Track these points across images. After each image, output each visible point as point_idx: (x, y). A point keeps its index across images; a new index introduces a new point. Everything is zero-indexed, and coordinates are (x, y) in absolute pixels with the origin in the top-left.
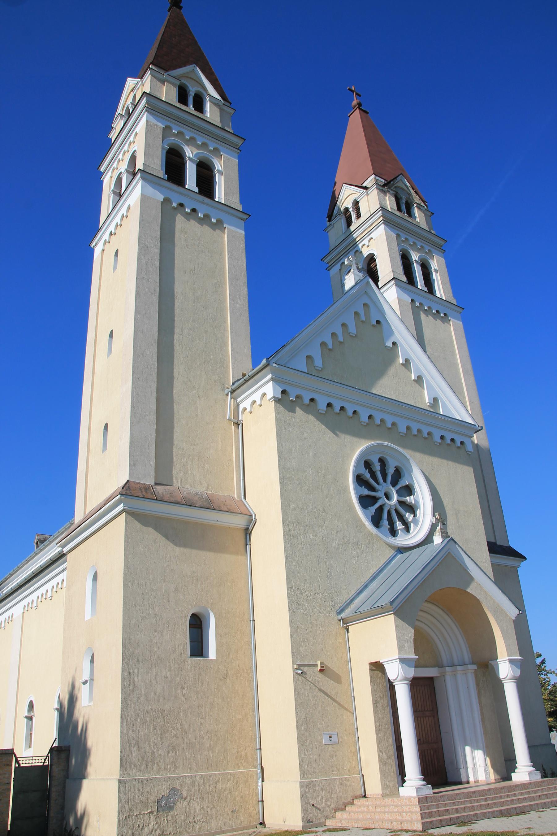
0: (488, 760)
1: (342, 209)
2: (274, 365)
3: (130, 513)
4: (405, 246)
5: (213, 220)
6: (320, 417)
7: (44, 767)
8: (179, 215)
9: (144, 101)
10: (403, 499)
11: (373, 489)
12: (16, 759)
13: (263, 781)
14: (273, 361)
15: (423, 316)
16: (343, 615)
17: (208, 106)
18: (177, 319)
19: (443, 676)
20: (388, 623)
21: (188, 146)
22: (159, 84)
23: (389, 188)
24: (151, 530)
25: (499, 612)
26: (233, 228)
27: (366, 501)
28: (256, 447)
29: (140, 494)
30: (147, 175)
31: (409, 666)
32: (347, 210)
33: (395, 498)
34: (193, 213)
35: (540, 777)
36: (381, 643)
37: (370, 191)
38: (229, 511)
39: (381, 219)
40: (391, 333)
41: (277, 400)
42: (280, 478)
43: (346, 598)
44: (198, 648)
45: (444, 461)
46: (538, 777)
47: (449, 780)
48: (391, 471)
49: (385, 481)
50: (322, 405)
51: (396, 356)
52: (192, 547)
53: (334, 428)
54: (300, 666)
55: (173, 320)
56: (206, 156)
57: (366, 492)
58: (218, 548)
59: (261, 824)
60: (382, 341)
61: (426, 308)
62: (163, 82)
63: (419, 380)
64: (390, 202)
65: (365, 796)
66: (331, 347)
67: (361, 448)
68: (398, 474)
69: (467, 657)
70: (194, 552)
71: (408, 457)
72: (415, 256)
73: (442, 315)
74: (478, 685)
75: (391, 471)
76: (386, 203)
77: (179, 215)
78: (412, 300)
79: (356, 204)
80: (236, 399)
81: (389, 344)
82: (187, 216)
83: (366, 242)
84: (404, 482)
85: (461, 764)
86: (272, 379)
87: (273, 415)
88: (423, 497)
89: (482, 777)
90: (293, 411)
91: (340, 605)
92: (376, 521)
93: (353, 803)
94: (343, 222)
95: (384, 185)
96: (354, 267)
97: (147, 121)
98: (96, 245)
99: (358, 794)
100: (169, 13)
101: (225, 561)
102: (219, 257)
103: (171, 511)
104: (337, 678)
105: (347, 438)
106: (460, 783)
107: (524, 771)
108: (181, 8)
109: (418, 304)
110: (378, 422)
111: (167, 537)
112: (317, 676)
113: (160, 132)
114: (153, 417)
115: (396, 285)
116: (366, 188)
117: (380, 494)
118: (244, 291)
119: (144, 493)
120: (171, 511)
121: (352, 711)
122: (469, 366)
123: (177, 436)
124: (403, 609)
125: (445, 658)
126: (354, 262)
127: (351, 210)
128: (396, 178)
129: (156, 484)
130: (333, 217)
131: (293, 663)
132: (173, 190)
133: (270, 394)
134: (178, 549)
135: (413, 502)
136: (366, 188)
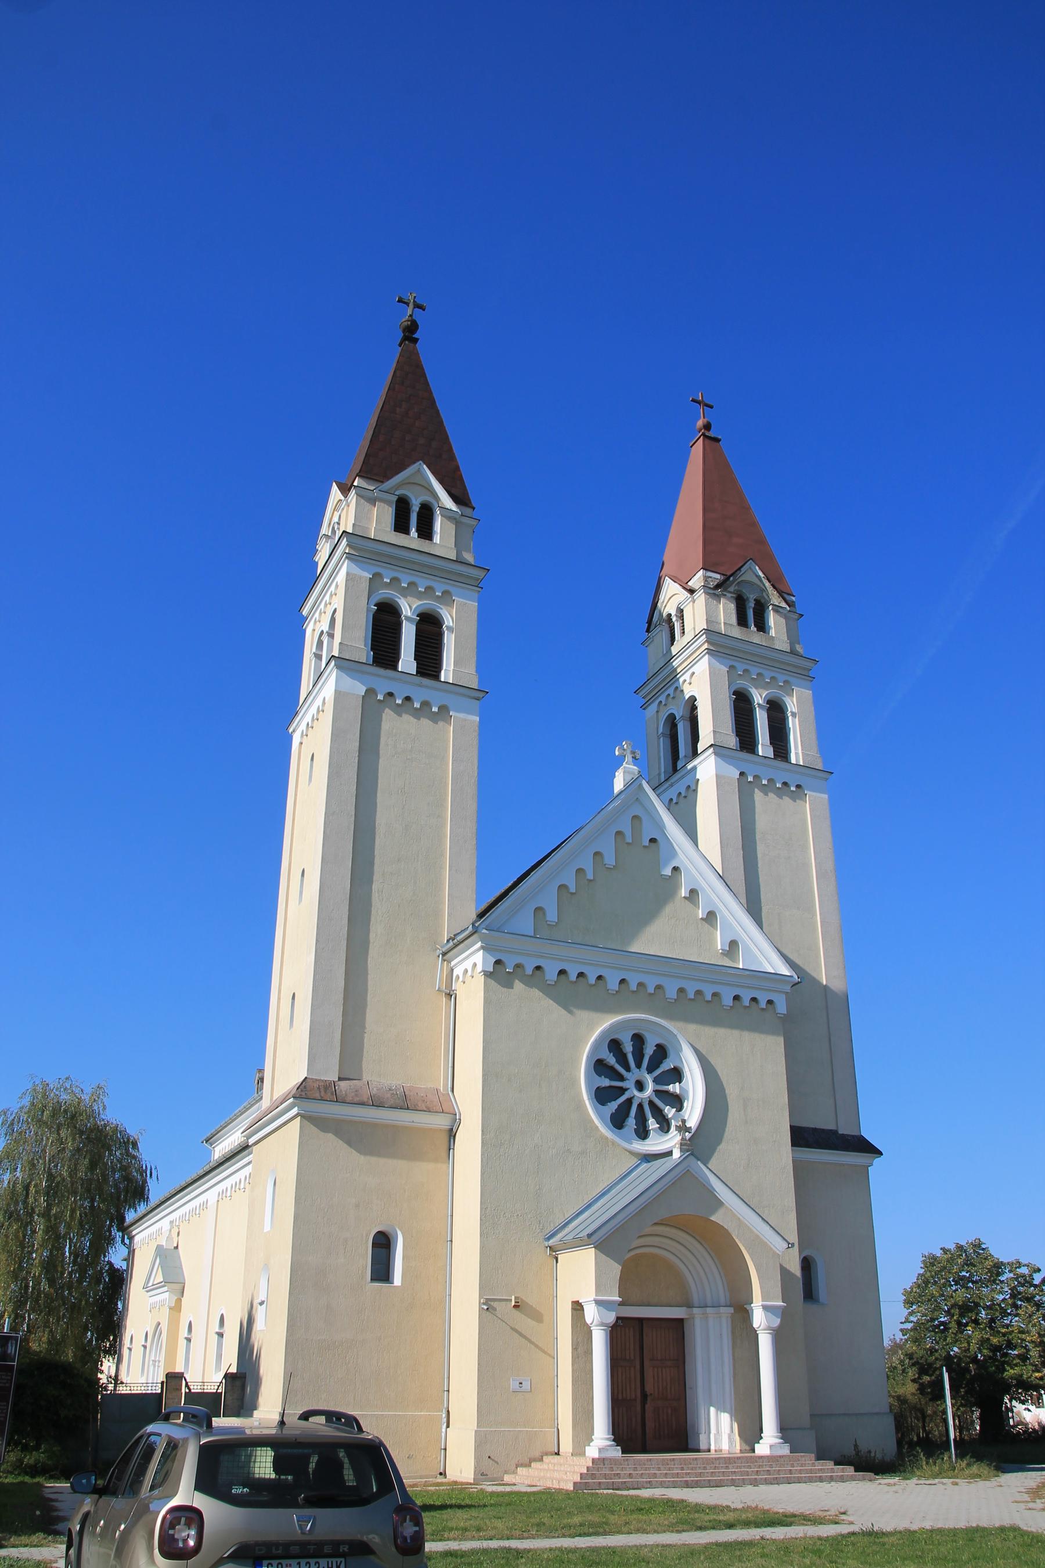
1: (665, 615)
2: (484, 931)
3: (306, 1117)
4: (741, 683)
5: (435, 709)
6: (548, 990)
7: (217, 1395)
8: (387, 710)
9: (344, 542)
10: (664, 1088)
11: (622, 1078)
12: (187, 1383)
13: (448, 1426)
14: (483, 926)
15: (758, 795)
16: (551, 1242)
17: (438, 523)
18: (377, 861)
19: (692, 1317)
20: (588, 1256)
21: (405, 597)
22: (367, 506)
23: (725, 590)
24: (330, 1136)
25: (758, 1245)
26: (461, 715)
27: (602, 1096)
28: (459, 1031)
29: (317, 1095)
30: (342, 662)
32: (670, 615)
33: (650, 1087)
34: (408, 703)
35: (788, 1452)
36: (581, 1280)
37: (696, 595)
38: (429, 1110)
39: (706, 646)
40: (673, 854)
41: (487, 974)
42: (483, 1076)
43: (559, 1220)
44: (382, 1272)
45: (736, 1033)
46: (785, 1450)
47: (690, 1446)
48: (649, 1050)
49: (639, 1066)
50: (551, 974)
51: (676, 887)
52: (379, 1155)
53: (567, 1004)
54: (487, 1302)
55: (372, 864)
56: (428, 606)
57: (606, 1082)
58: (414, 1155)
59: (441, 1474)
61: (765, 782)
62: (372, 501)
63: (711, 917)
64: (725, 611)
65: (558, 1454)
66: (573, 890)
68: (661, 1052)
69: (722, 1296)
70: (382, 1161)
71: (675, 1032)
72: (758, 697)
73: (793, 789)
74: (733, 1333)
75: (649, 1050)
76: (718, 615)
77: (387, 710)
78: (742, 774)
79: (680, 612)
80: (449, 962)
81: (667, 871)
82: (398, 710)
83: (687, 676)
84: (668, 1065)
85: (703, 1427)
86: (482, 948)
87: (481, 994)
88: (694, 1088)
89: (725, 1446)
90: (766, 794)
91: (550, 1229)
92: (618, 1121)
93: (541, 1460)
94: (665, 635)
95: (717, 587)
96: (629, 758)
97: (348, 574)
98: (294, 731)
99: (550, 1450)
100: (400, 349)
101: (421, 1171)
102: (441, 756)
103: (356, 1112)
104: (537, 1316)
105: (583, 1015)
106: (698, 1451)
107: (769, 1442)
108: (416, 340)
109: (750, 779)
110: (633, 987)
111: (349, 1143)
112: (509, 1312)
113: (365, 586)
114: (340, 996)
115: (716, 753)
116: (692, 591)
117: (629, 1084)
118: (471, 806)
119: (323, 1093)
120: (356, 1112)
121: (554, 1357)
122: (830, 865)
124: (605, 1242)
125: (695, 1299)
126: (628, 751)
127: (674, 619)
128: (739, 569)
129: (340, 1079)
130: (652, 627)
131: (480, 1297)
132: (379, 676)
133: (479, 968)
134: (362, 1157)
135: (678, 1091)
136: (692, 591)
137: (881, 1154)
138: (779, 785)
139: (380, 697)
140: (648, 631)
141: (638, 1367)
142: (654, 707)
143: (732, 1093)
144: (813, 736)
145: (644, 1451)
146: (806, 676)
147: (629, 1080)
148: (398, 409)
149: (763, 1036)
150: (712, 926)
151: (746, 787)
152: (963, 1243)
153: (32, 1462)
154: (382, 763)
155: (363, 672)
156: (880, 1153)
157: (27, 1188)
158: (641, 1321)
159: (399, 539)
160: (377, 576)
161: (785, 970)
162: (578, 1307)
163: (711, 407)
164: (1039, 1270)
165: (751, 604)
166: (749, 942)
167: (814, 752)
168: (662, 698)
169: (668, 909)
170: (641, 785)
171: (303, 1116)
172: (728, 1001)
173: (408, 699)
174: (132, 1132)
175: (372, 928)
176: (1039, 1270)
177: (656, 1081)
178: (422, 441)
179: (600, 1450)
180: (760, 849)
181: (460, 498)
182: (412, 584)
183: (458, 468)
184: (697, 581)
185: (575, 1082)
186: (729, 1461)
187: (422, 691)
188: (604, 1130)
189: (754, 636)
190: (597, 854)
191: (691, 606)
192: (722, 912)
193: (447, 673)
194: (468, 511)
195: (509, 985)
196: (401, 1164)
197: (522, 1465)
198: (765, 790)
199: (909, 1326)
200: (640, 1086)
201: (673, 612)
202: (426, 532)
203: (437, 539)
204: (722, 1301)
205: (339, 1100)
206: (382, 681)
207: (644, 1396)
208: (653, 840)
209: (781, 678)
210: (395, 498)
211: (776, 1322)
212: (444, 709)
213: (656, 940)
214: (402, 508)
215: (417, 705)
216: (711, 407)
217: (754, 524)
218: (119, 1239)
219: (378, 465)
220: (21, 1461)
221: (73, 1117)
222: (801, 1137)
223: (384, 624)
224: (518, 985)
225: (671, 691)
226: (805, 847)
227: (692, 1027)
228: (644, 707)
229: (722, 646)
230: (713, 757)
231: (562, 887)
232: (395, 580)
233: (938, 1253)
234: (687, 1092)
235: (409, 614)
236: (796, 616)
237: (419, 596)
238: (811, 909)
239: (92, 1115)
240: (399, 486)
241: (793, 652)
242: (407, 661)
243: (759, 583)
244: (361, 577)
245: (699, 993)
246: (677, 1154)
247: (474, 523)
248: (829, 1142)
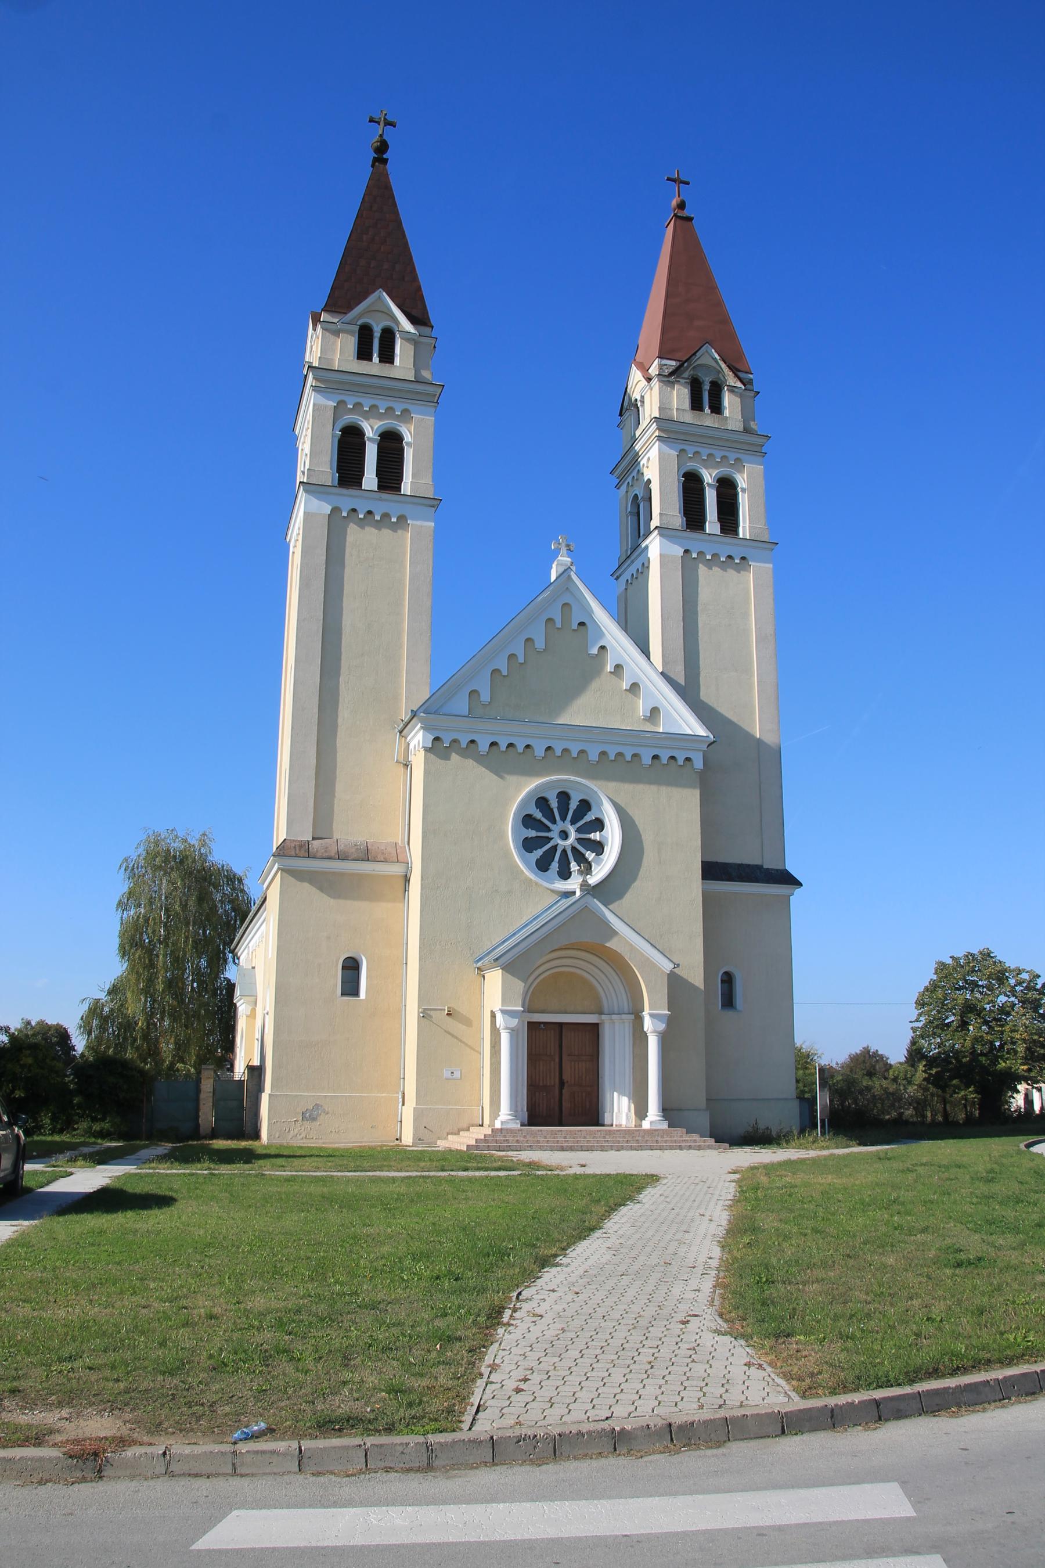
0: (632, 1106)
4: (691, 466)
5: (394, 520)
6: (480, 759)
13: (403, 1104)
15: (702, 569)
16: (479, 964)
18: (343, 657)
20: (495, 978)
21: (367, 419)
22: (332, 337)
24: (306, 885)
25: (648, 964)
26: (418, 523)
27: (528, 845)
29: (293, 853)
31: (513, 1017)
33: (573, 835)
34: (369, 516)
36: (495, 995)
38: (386, 861)
40: (600, 634)
41: (427, 750)
44: (351, 988)
45: (654, 788)
46: (665, 1125)
49: (563, 819)
50: (483, 746)
51: (603, 665)
52: (346, 898)
55: (339, 660)
57: (532, 833)
60: (586, 647)
62: (336, 333)
63: (634, 687)
64: (680, 396)
66: (505, 673)
67: (527, 790)
68: (585, 806)
70: (349, 902)
71: (595, 789)
74: (634, 1035)
76: (671, 402)
77: (351, 525)
78: (686, 551)
79: (642, 397)
81: (595, 651)
82: (362, 524)
84: (590, 817)
86: (422, 728)
88: (613, 835)
89: (624, 1122)
92: (542, 866)
93: (468, 1130)
95: (671, 374)
96: (564, 550)
101: (381, 909)
104: (468, 1022)
105: (512, 779)
106: (603, 1125)
109: (694, 555)
111: (321, 889)
112: (443, 1019)
113: (330, 414)
117: (554, 834)
121: (480, 1053)
122: (770, 629)
123: (339, 787)
128: (695, 354)
129: (314, 839)
131: (419, 1007)
137: (801, 885)
138: (723, 559)
139: (344, 514)
140: (621, 415)
141: (557, 1060)
142: (624, 487)
143: (648, 839)
144: (762, 509)
145: (561, 1124)
146: (758, 452)
147: (554, 832)
148: (365, 237)
149: (680, 790)
150: (635, 695)
151: (689, 563)
152: (975, 952)
153: (98, 1129)
154: (348, 571)
156: (800, 884)
157: (147, 920)
158: (561, 1025)
159: (363, 367)
160: (341, 403)
161: (701, 731)
162: (493, 1015)
163: (688, 183)
164: (1039, 976)
165: (707, 387)
166: (669, 708)
167: (761, 525)
168: (629, 480)
169: (595, 685)
170: (569, 577)
171: (282, 870)
172: (647, 760)
173: (370, 512)
174: (238, 870)
175: (340, 714)
176: (1039, 976)
177: (578, 831)
178: (386, 266)
179: (502, 1123)
180: (702, 619)
181: (419, 319)
182: (373, 407)
183: (419, 289)
184: (654, 370)
185: (502, 835)
186: (628, 1132)
187: (386, 504)
188: (529, 874)
189: (707, 418)
190: (528, 640)
191: (651, 394)
192: (645, 683)
193: (407, 486)
194: (426, 330)
195: (447, 758)
196: (364, 905)
197: (452, 1134)
198: (709, 564)
199: (920, 1024)
200: (564, 835)
201: (639, 399)
202: (387, 357)
203: (397, 361)
204: (626, 1010)
205: (309, 855)
206: (347, 499)
207: (562, 1084)
208: (582, 624)
209: (732, 456)
210: (357, 328)
211: (662, 1027)
212: (402, 519)
213: (583, 712)
214: (365, 334)
215: (377, 518)
216: (688, 183)
217: (719, 304)
218: (230, 959)
219: (342, 298)
220: (91, 1128)
221: (182, 862)
222: (712, 871)
223: (349, 446)
224: (454, 757)
225: (635, 473)
226: (746, 615)
227: (612, 785)
228: (618, 487)
229: (672, 432)
230: (658, 537)
231: (496, 671)
232: (358, 405)
233: (950, 961)
234: (607, 839)
235: (371, 435)
236: (752, 394)
237: (381, 416)
238: (748, 671)
239: (203, 858)
241: (747, 430)
242: (370, 479)
243: (714, 365)
244: (326, 406)
246: (578, 893)
247: (433, 341)
248: (744, 875)
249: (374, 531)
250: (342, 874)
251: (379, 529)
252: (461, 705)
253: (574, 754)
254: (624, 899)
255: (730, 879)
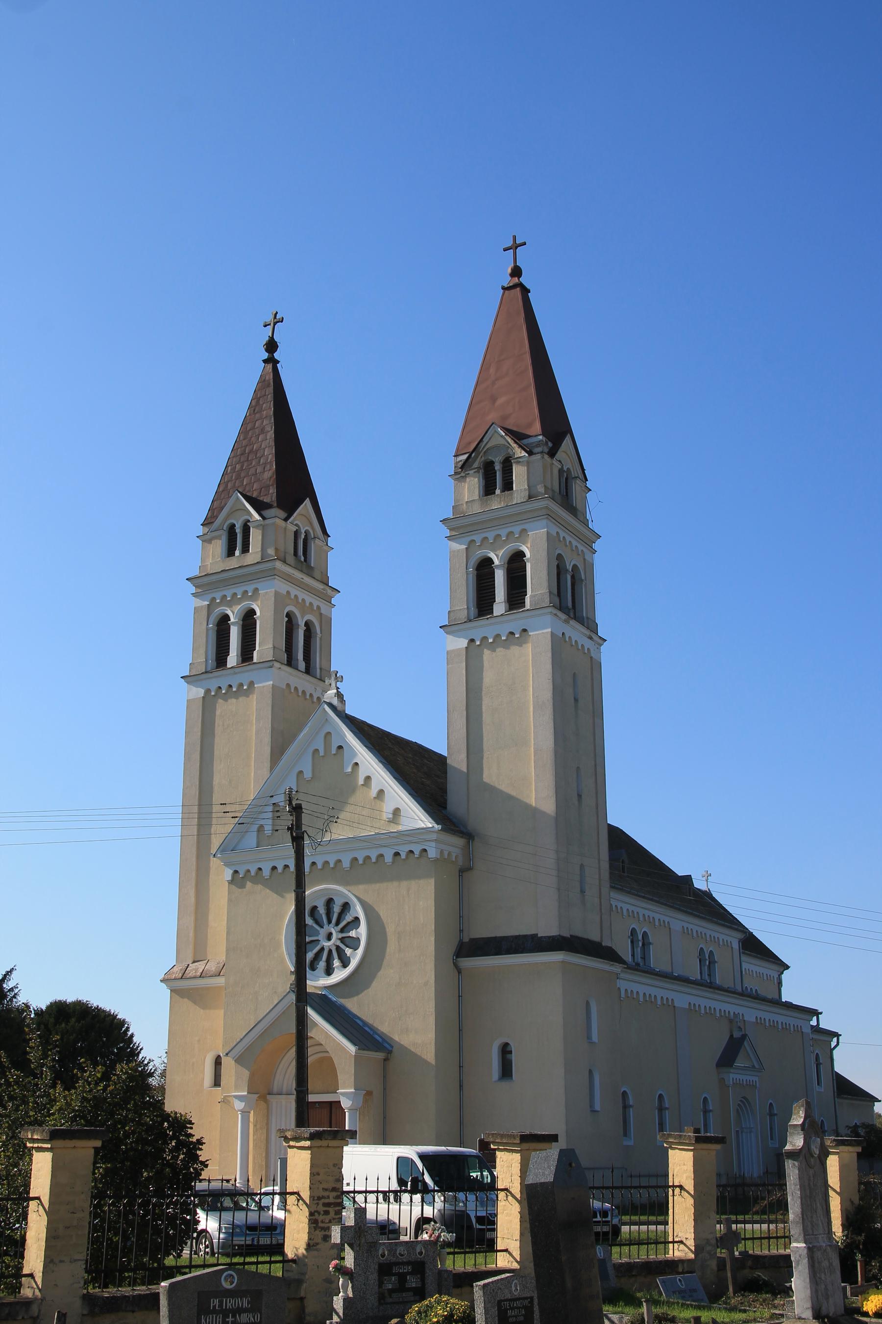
6: (267, 883)
15: (487, 652)
24: (186, 1000)
40: (354, 754)
50: (266, 872)
82: (226, 697)
111: (195, 1002)
113: (205, 612)
152: (135, 1039)
154: (217, 740)
155: (201, 680)
159: (233, 563)
172: (389, 858)
200: (329, 937)
212: (251, 684)
224: (249, 884)
240: (226, 519)
245: (368, 857)
249: (234, 700)
250: (208, 989)
251: (237, 698)
252: (251, 840)
253: (374, 860)
254: (370, 991)
255: (509, 951)
